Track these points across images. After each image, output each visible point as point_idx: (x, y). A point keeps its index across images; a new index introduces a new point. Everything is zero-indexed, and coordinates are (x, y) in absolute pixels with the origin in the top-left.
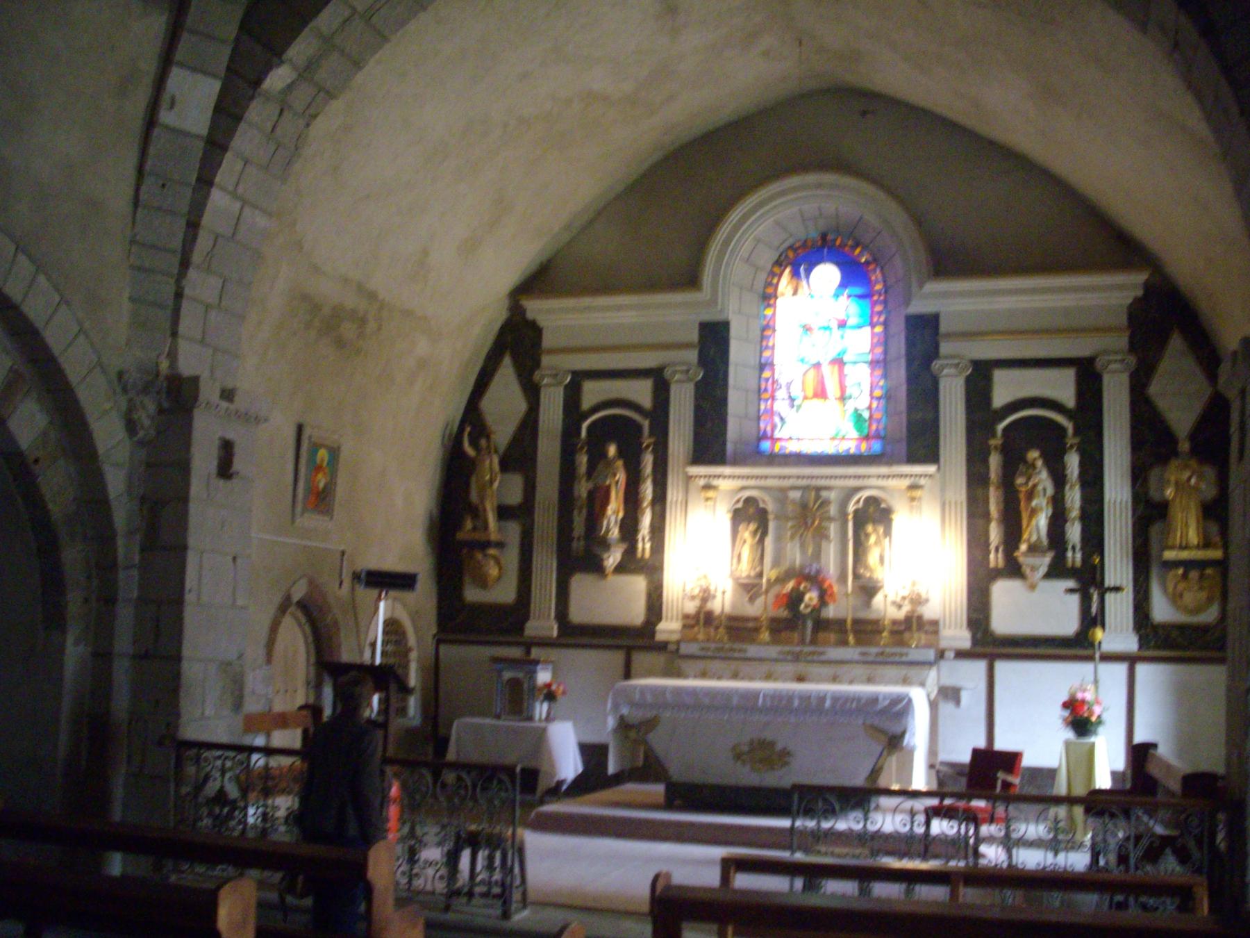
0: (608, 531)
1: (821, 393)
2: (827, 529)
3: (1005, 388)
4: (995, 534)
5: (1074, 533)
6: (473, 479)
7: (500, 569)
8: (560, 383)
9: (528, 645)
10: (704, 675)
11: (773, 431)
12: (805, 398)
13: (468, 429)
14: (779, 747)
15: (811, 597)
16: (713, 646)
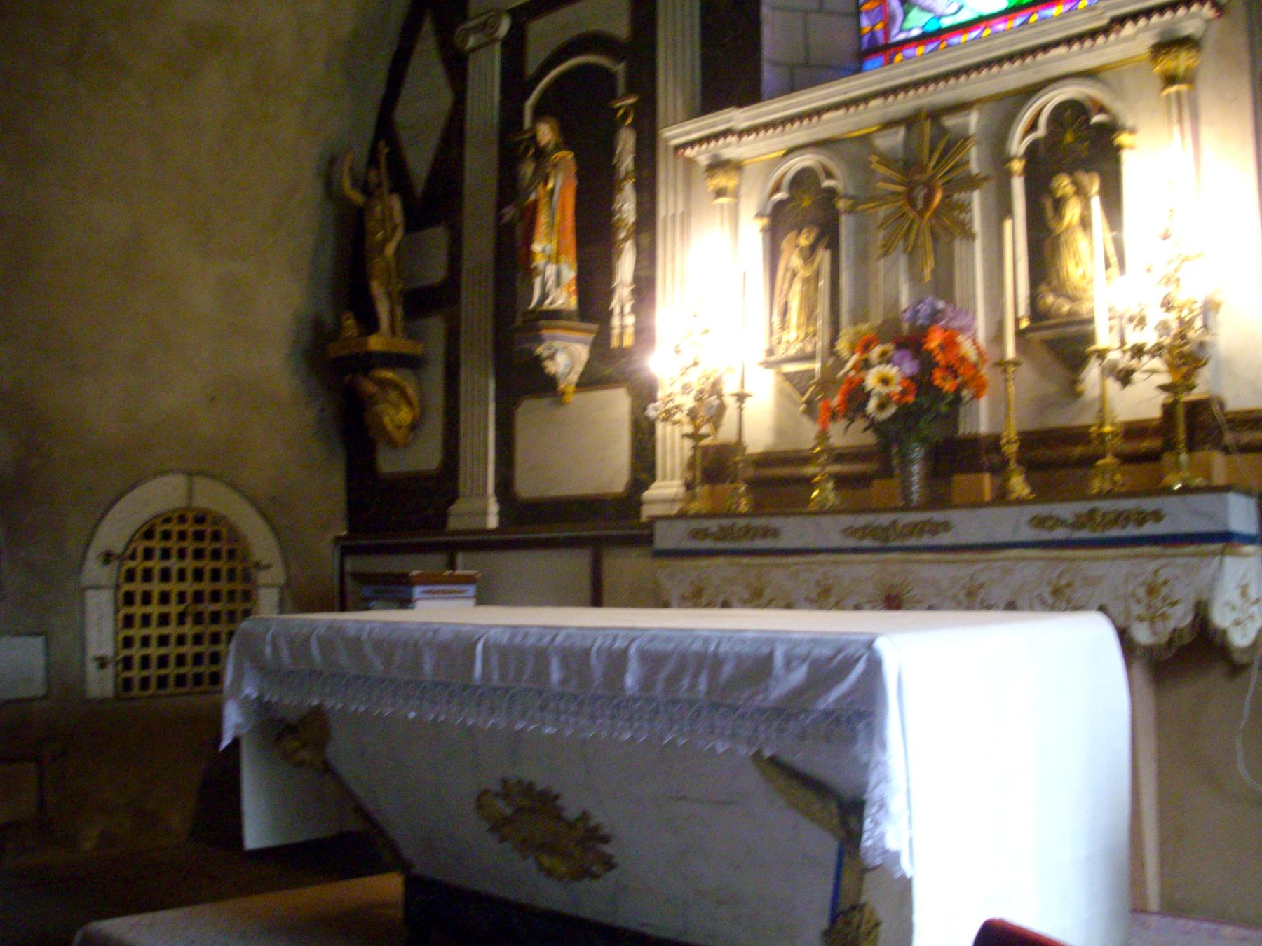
2: (965, 207)
10: (697, 598)
11: (886, 32)
16: (713, 525)
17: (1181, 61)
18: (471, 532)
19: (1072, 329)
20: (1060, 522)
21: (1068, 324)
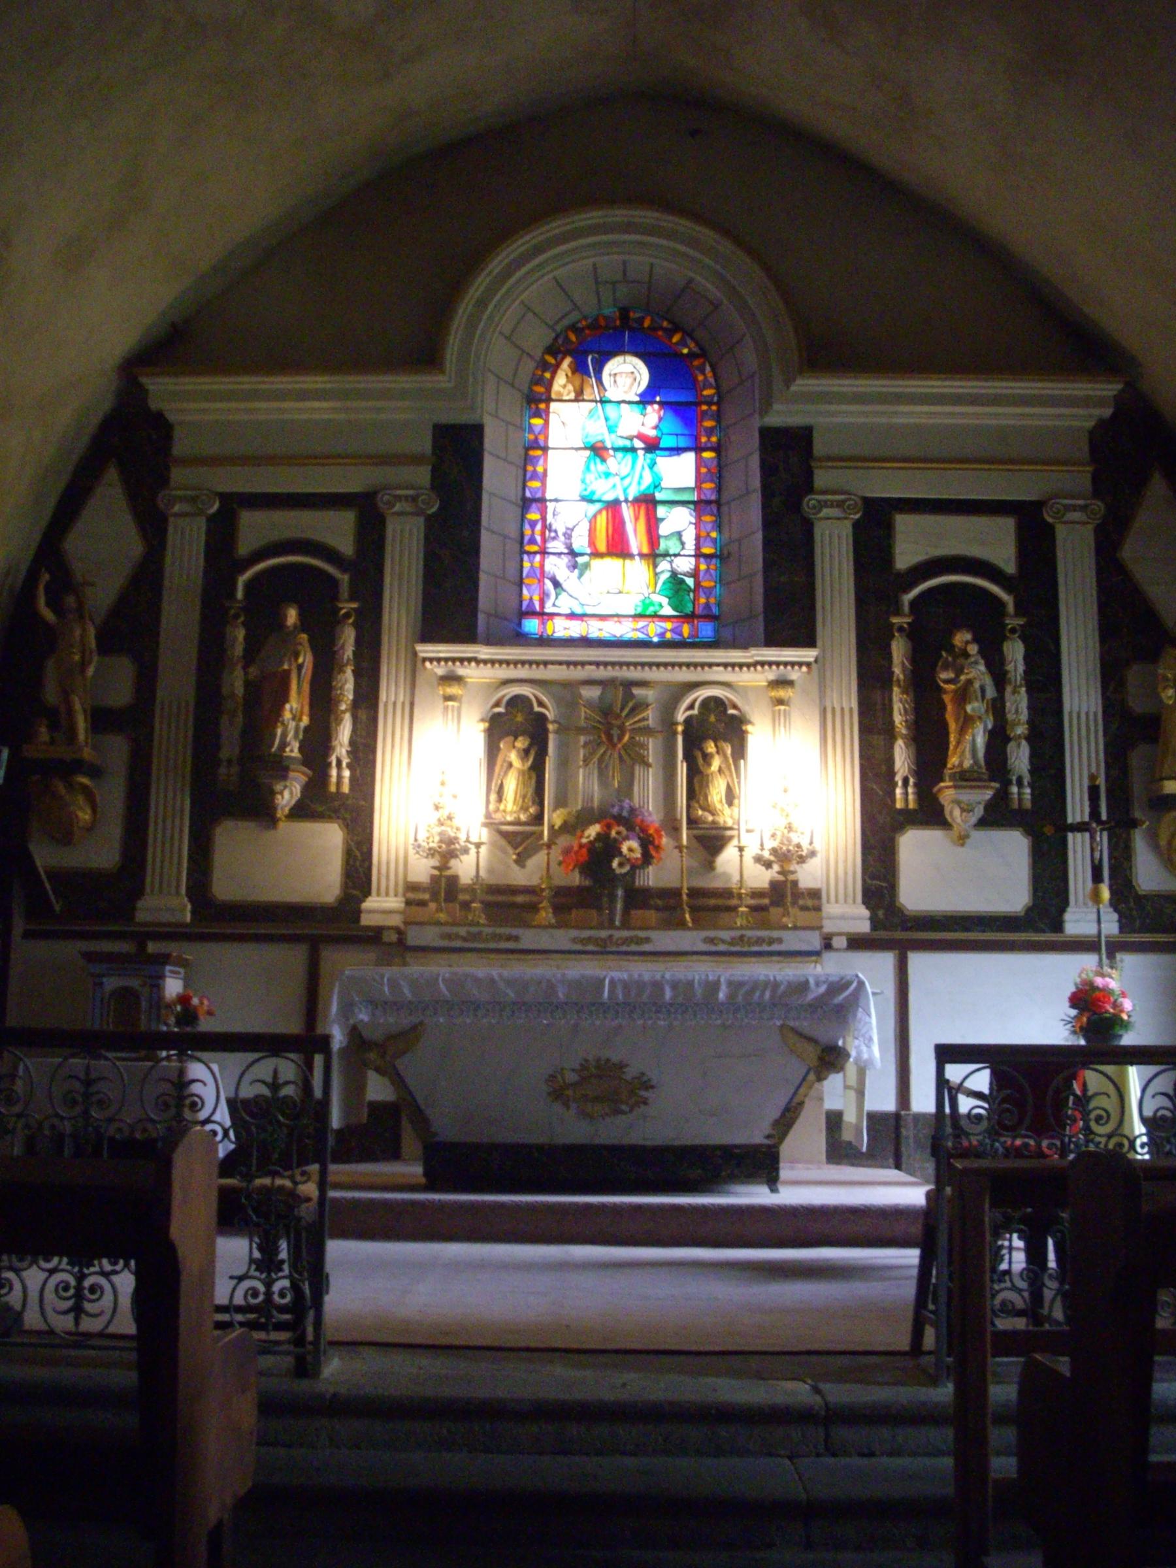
0: (284, 745)
1: (618, 547)
2: (644, 746)
3: (912, 542)
4: (902, 759)
5: (1020, 758)
6: (50, 664)
7: (94, 811)
8: (201, 512)
9: (141, 938)
11: (542, 603)
12: (596, 554)
13: (46, 577)
14: (630, 1073)
15: (631, 847)
16: (462, 931)
17: (782, 693)
18: (169, 925)
19: (714, 832)
20: (723, 941)
21: (712, 829)
